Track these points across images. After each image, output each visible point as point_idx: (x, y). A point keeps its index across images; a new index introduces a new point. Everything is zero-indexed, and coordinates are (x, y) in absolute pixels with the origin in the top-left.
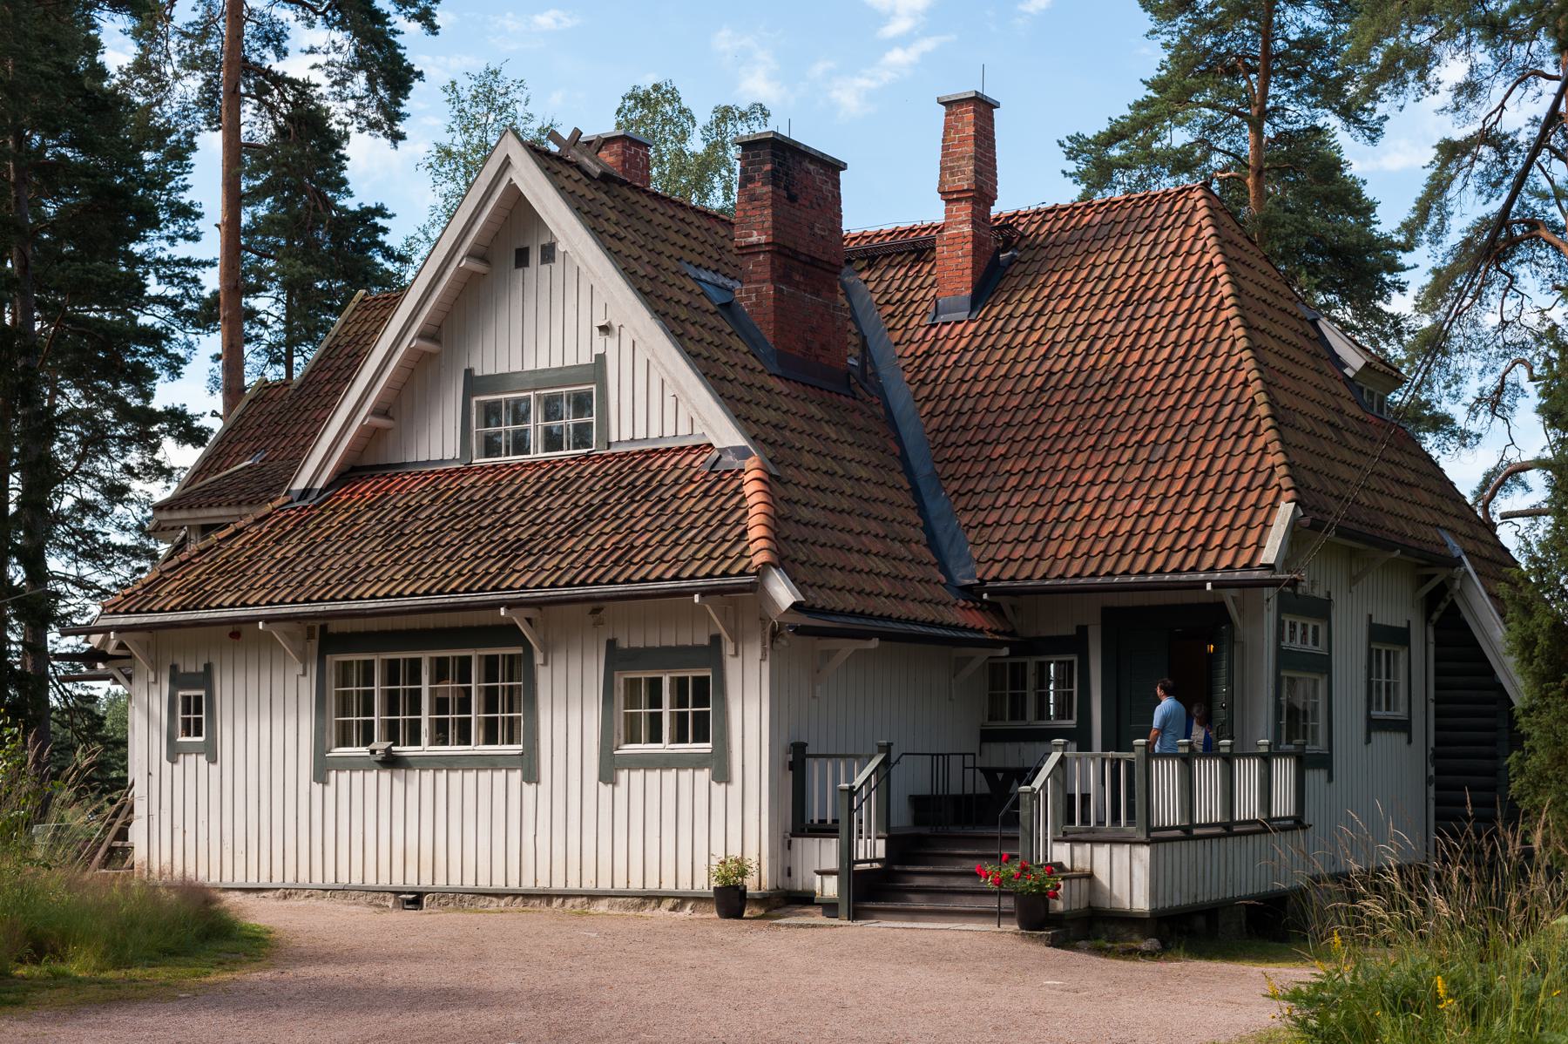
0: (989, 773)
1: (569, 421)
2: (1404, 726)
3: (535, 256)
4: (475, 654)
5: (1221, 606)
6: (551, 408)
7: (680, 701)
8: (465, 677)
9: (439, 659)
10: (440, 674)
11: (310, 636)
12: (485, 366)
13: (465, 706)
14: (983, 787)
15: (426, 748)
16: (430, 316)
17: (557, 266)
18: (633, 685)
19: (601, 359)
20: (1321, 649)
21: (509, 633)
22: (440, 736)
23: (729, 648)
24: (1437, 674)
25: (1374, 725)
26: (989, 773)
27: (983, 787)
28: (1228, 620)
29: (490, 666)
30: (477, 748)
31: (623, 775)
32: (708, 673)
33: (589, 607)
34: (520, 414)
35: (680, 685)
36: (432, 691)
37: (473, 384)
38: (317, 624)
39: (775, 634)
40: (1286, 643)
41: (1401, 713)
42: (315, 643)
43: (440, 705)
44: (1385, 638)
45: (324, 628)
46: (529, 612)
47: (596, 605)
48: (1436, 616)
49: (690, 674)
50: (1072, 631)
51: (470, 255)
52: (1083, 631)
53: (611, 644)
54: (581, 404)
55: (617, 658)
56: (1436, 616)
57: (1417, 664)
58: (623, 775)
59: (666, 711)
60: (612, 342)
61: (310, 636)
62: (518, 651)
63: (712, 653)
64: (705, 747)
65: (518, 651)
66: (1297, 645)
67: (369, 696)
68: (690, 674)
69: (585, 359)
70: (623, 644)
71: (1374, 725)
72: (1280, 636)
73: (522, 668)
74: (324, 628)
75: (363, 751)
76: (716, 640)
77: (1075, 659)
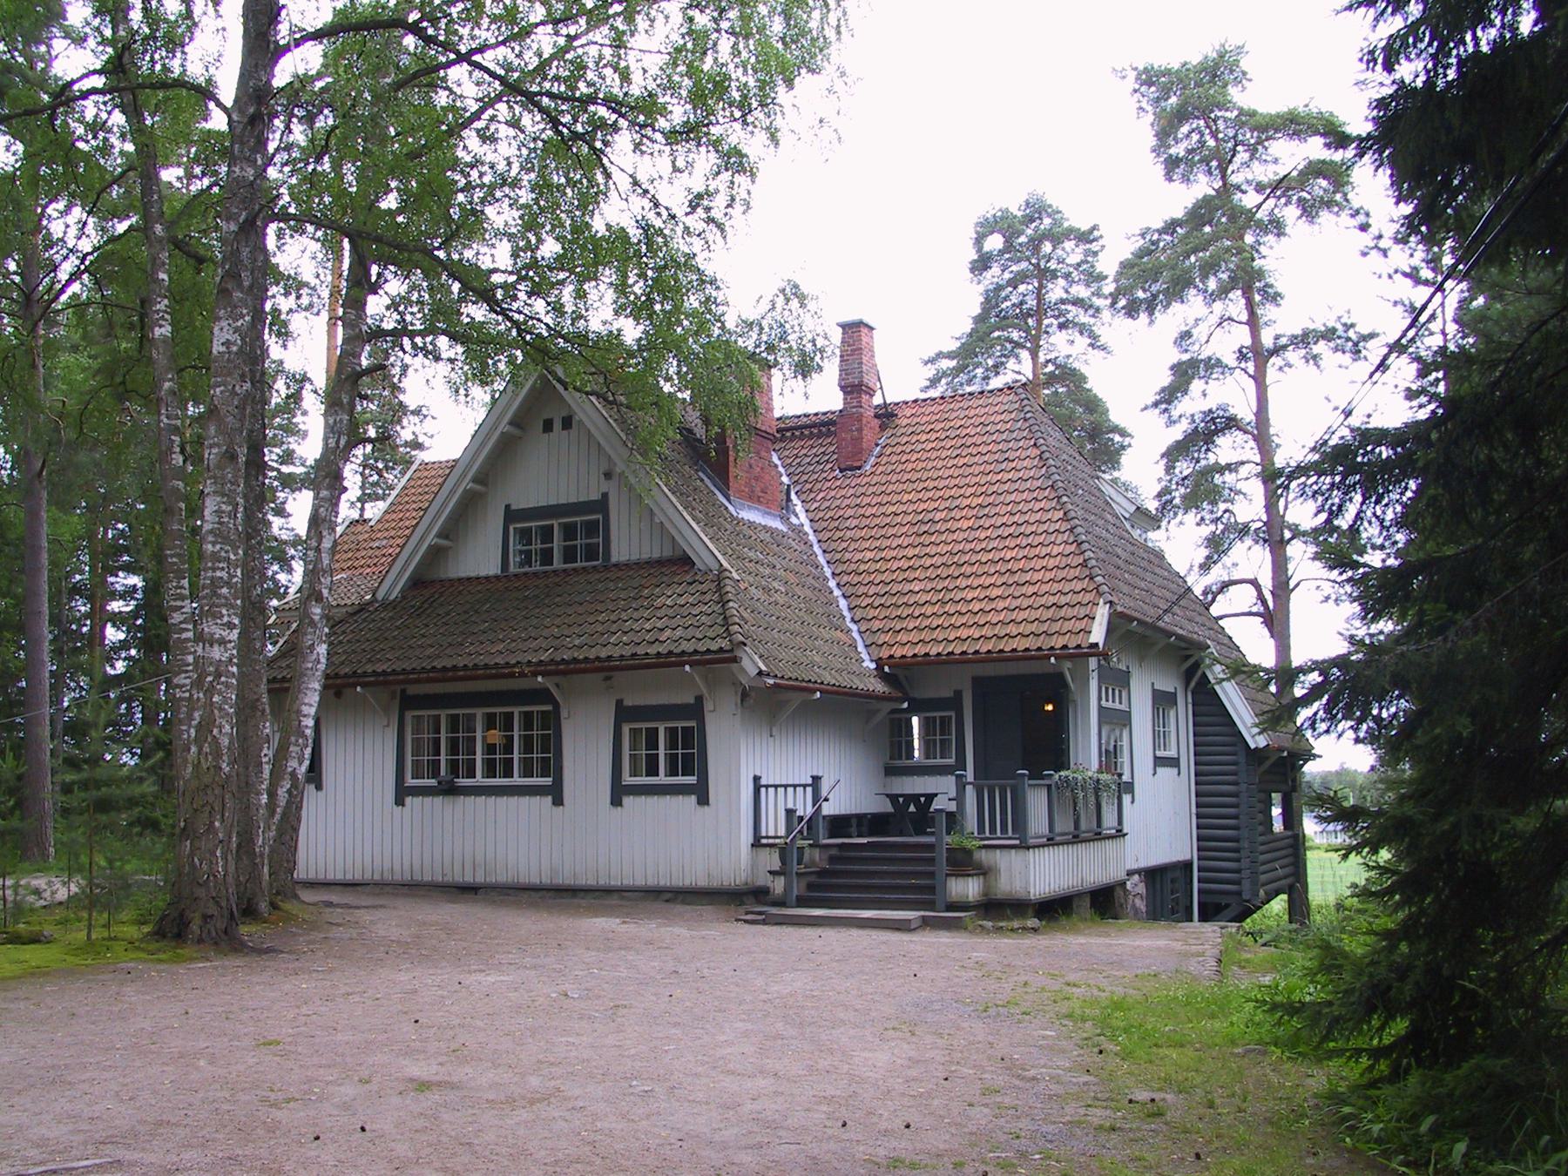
0: (893, 798)
1: (537, 546)
2: (1173, 762)
3: (557, 425)
4: (516, 711)
5: (1061, 676)
6: (569, 532)
7: (672, 744)
8: (509, 726)
9: (526, 713)
10: (490, 723)
11: (393, 697)
12: (520, 504)
13: (508, 748)
14: (889, 809)
15: (479, 779)
16: (481, 466)
17: (574, 432)
18: (635, 733)
19: (605, 495)
20: (1123, 707)
21: (543, 695)
22: (490, 771)
23: (708, 706)
24: (1195, 725)
25: (1159, 762)
26: (893, 798)
27: (889, 809)
28: (1065, 685)
29: (527, 719)
30: (517, 780)
31: (408, 800)
32: (693, 724)
33: (603, 675)
34: (547, 534)
35: (672, 732)
36: (484, 738)
37: (511, 515)
38: (398, 688)
39: (745, 695)
40: (1103, 703)
41: (1172, 753)
42: (397, 701)
43: (490, 749)
44: (1163, 701)
45: (403, 691)
46: (557, 679)
47: (606, 669)
48: (1193, 684)
49: (680, 724)
50: (948, 694)
51: (511, 423)
52: (958, 694)
53: (619, 703)
54: (591, 528)
55: (624, 714)
56: (1193, 684)
57: (1181, 720)
58: (408, 800)
59: (662, 752)
60: (613, 484)
61: (393, 697)
62: (549, 708)
63: (696, 710)
64: (691, 780)
65: (549, 708)
66: (1110, 704)
67: (437, 742)
68: (680, 724)
69: (595, 496)
70: (628, 702)
71: (1159, 762)
72: (1100, 699)
73: (552, 722)
74: (403, 691)
75: (433, 782)
76: (699, 699)
77: (953, 714)
